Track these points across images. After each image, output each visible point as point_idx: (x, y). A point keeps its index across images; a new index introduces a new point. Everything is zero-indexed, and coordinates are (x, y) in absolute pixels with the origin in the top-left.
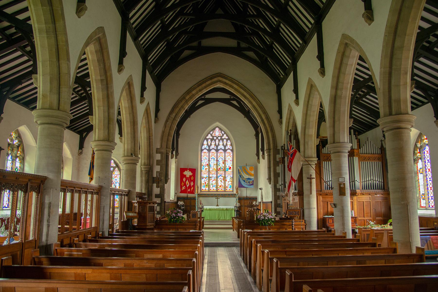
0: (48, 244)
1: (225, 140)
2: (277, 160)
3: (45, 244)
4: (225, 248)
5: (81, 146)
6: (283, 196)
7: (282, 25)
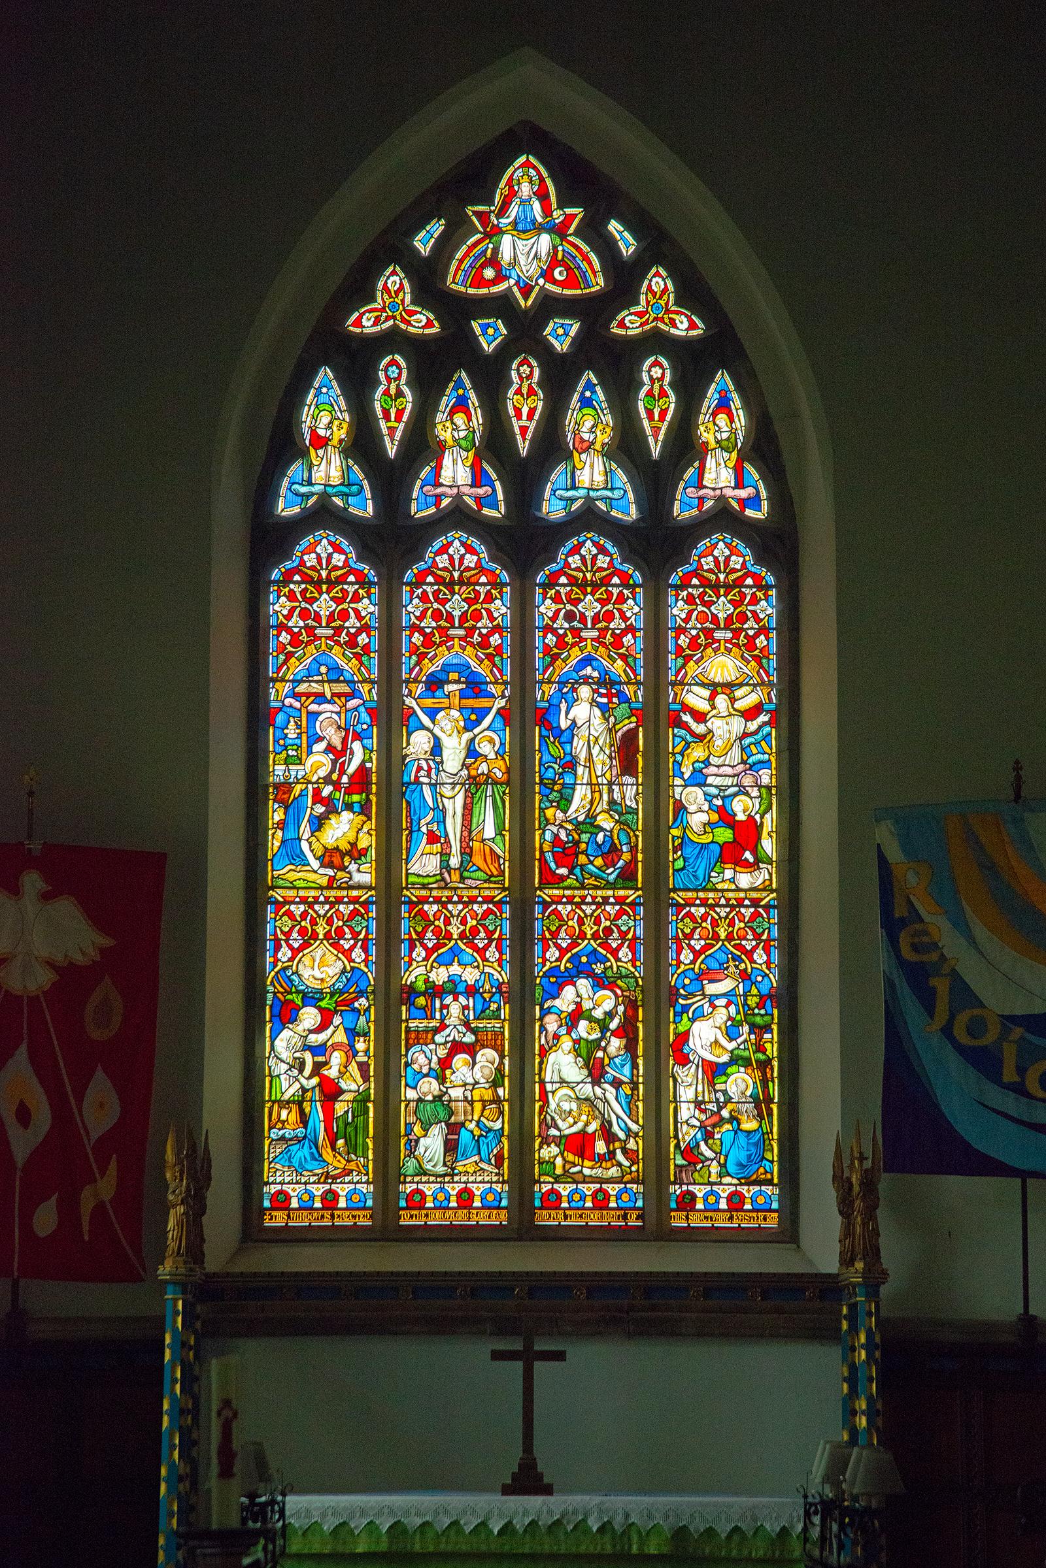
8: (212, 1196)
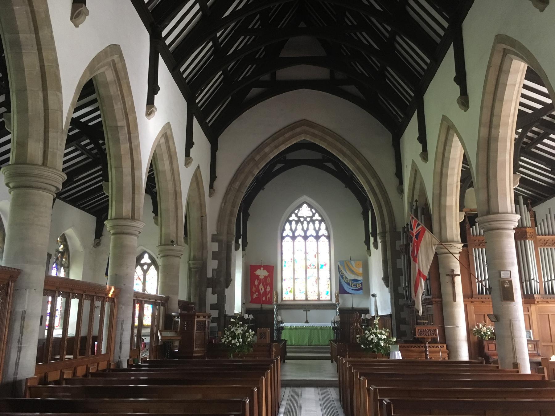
0: (18, 379)
1: (317, 223)
2: (397, 249)
3: (12, 380)
4: (316, 389)
5: (99, 232)
6: (408, 306)
7: (398, 39)
8: (279, 297)
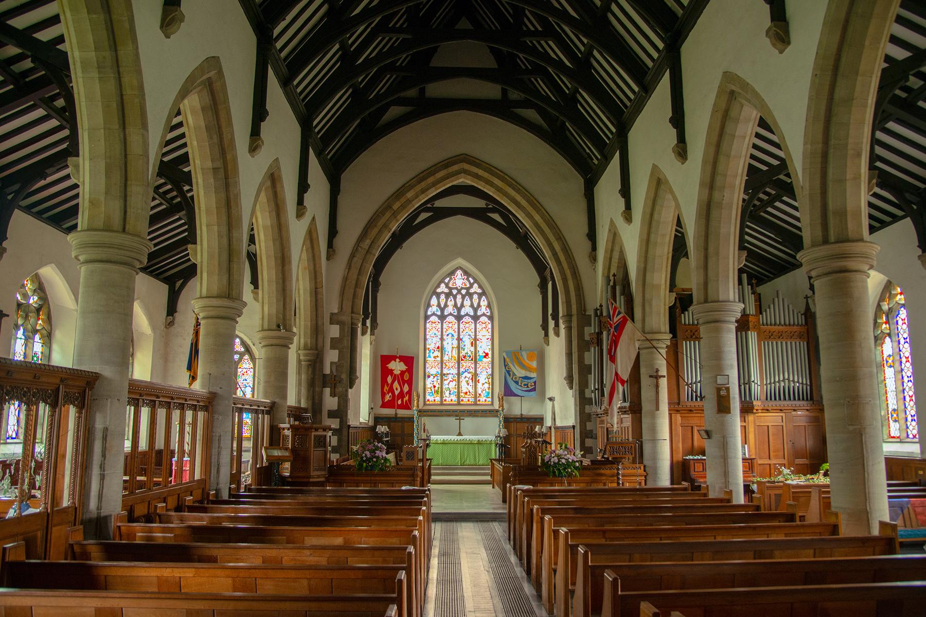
0: (102, 515)
1: (475, 297)
2: (586, 339)
3: (95, 516)
4: (476, 524)
5: (172, 309)
6: (597, 415)
7: (595, 53)
